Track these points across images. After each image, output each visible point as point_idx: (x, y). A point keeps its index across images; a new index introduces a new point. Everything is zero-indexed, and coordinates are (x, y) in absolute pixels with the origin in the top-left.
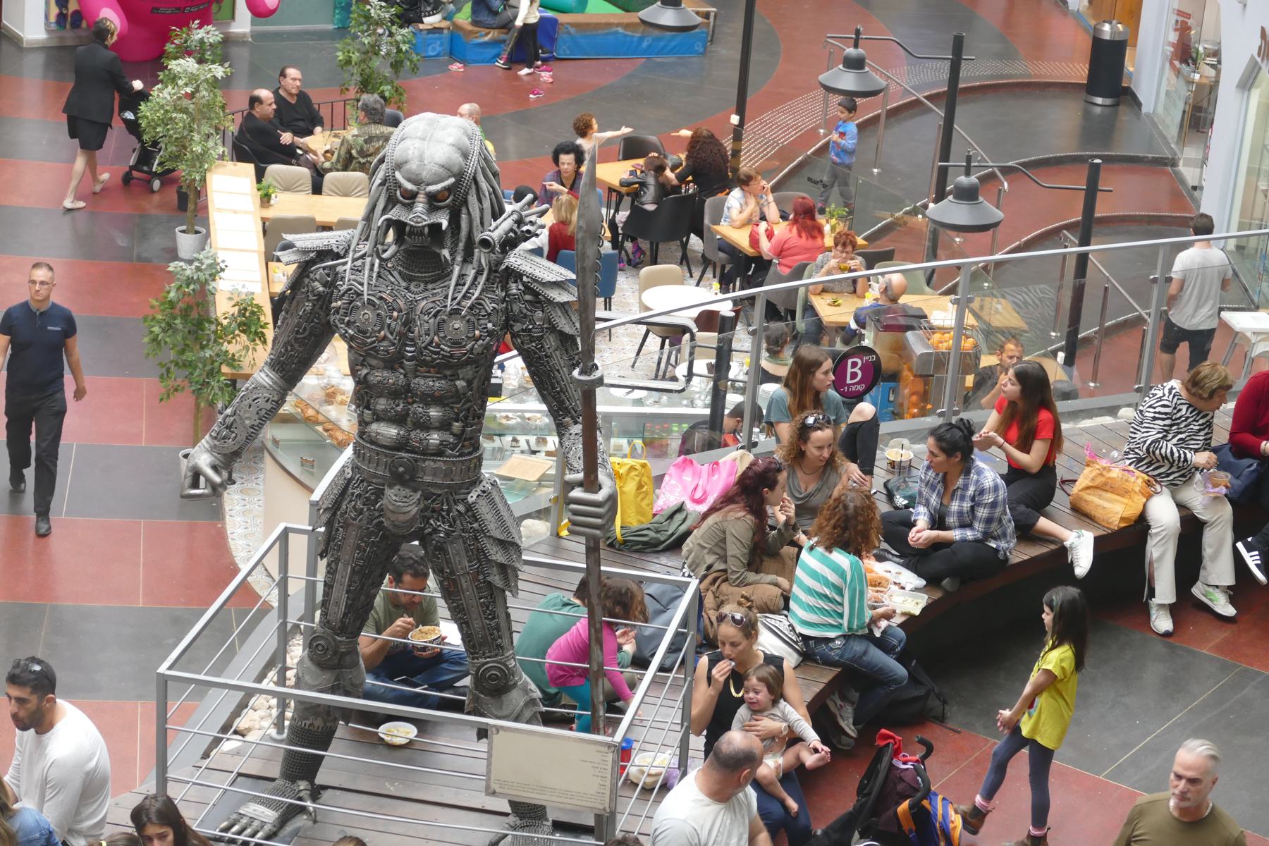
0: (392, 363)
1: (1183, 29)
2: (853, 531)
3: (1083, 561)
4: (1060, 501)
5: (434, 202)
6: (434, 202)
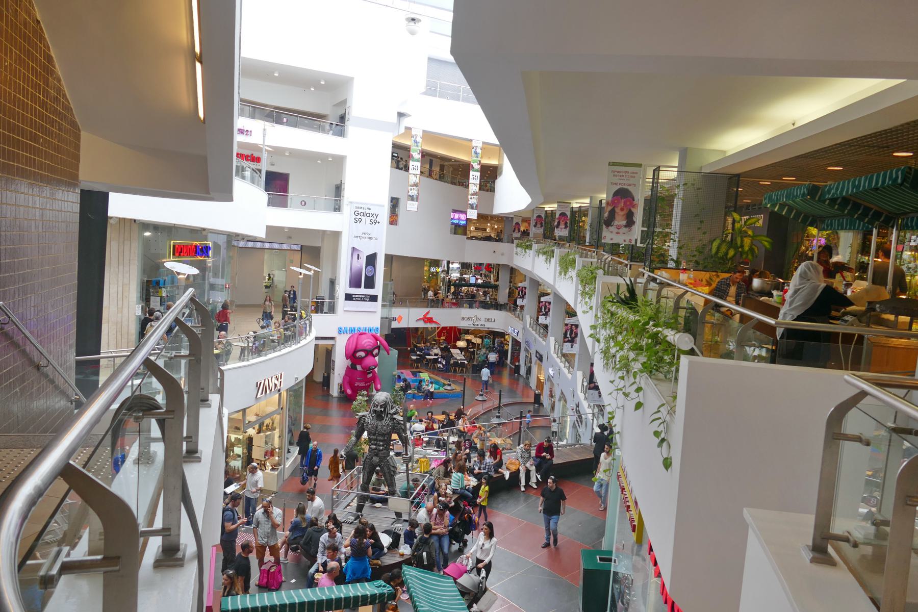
0: (374, 435)
1: (551, 391)
2: (461, 470)
3: (507, 477)
4: (504, 467)
5: (381, 406)
6: (381, 406)
